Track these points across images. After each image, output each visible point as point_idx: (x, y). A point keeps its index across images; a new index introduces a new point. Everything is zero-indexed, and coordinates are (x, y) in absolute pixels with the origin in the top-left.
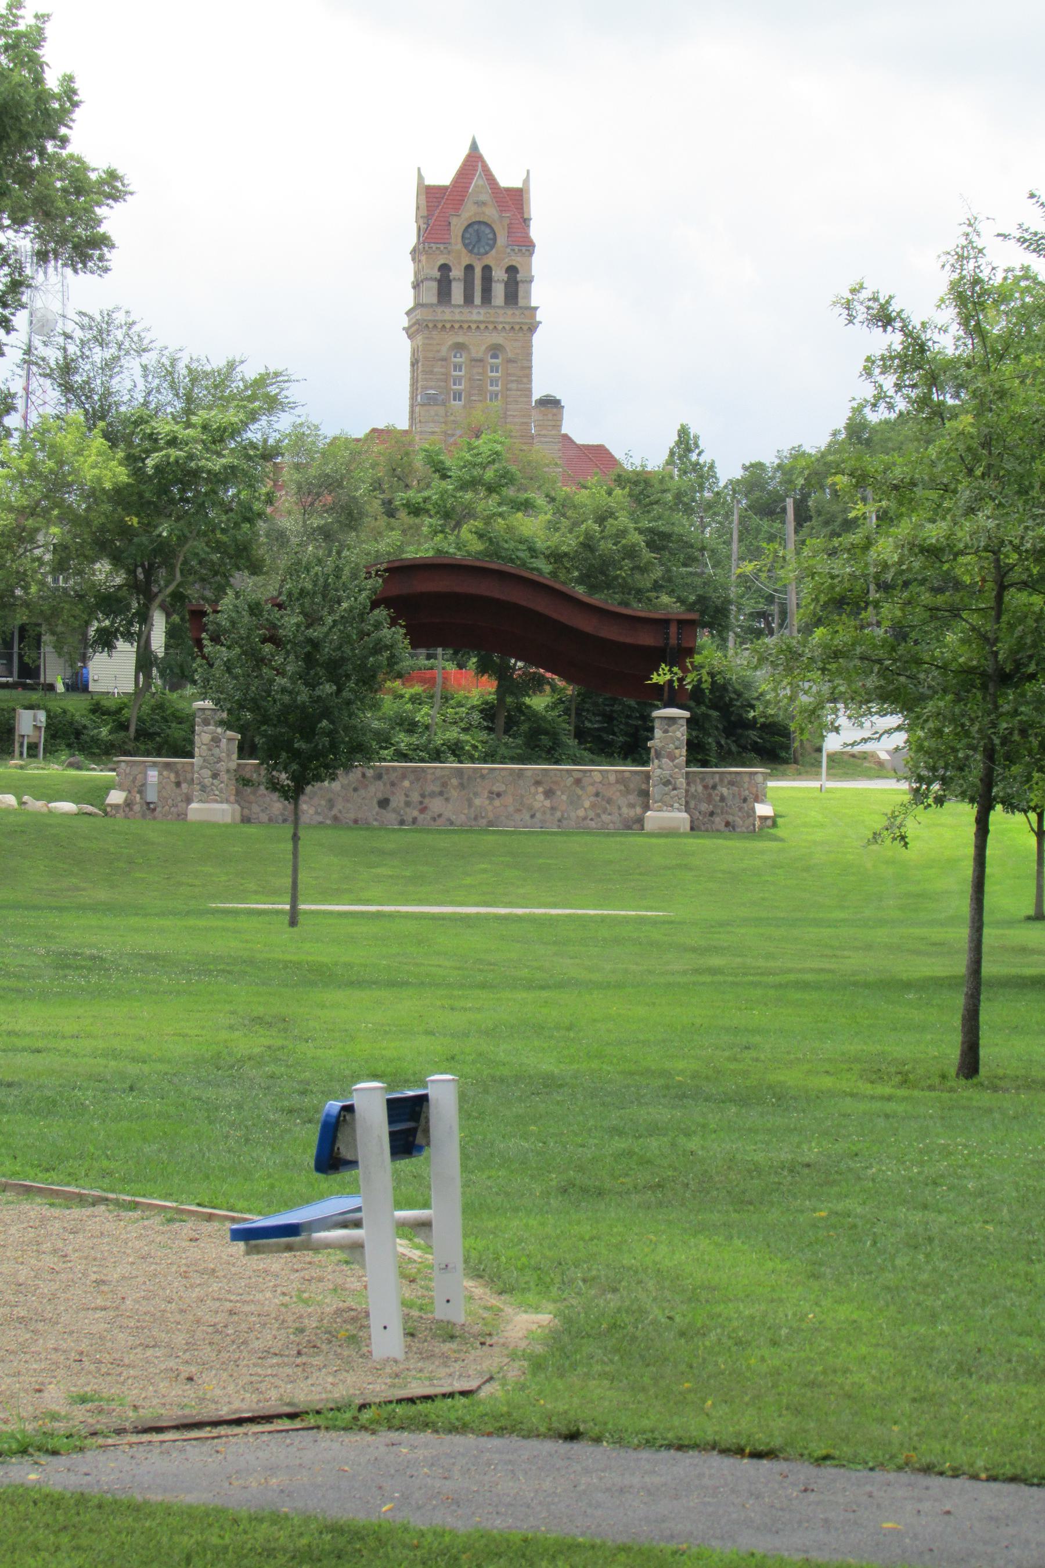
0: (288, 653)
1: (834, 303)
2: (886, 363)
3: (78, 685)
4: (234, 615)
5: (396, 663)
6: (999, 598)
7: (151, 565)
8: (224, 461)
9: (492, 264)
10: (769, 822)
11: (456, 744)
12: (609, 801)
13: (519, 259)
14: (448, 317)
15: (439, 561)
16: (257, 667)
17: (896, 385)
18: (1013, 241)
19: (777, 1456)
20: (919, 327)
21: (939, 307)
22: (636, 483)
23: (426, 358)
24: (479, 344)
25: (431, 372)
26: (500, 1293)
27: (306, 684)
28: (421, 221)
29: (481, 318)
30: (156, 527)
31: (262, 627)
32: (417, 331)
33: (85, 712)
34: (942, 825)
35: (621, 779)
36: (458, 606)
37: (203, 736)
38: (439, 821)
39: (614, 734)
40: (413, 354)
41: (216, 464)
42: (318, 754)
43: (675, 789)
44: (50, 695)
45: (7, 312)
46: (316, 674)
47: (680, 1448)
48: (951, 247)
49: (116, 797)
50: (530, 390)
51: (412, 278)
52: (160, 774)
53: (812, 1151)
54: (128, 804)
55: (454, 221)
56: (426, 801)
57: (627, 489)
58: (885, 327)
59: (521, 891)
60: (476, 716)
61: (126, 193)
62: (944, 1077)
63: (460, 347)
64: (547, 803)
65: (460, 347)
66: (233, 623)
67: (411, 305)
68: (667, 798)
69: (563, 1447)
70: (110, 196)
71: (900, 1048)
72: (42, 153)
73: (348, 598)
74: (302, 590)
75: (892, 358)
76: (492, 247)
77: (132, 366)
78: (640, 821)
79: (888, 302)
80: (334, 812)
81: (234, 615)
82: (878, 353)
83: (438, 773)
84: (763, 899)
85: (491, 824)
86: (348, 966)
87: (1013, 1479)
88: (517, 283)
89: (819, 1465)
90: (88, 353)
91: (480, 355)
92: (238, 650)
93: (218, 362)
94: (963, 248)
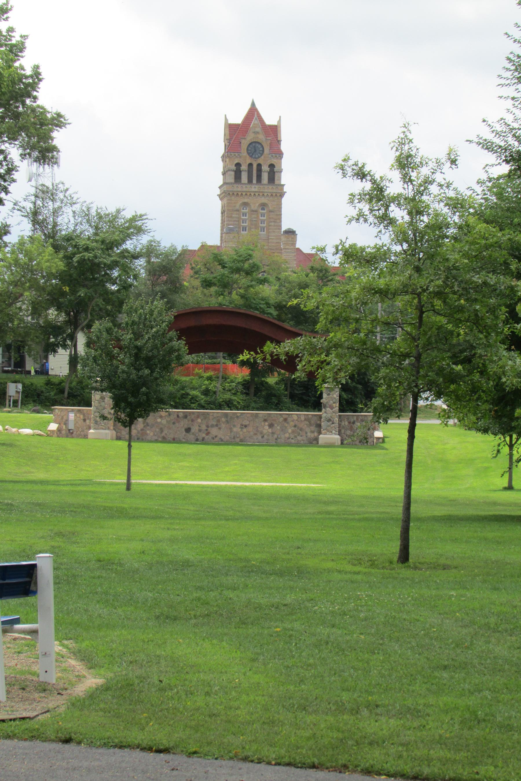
0: (126, 353)
1: (336, 167)
2: (362, 197)
3: (43, 371)
4: (98, 334)
5: (181, 359)
6: (421, 318)
7: (77, 311)
8: (112, 259)
9: (262, 163)
10: (381, 440)
11: (229, 401)
12: (301, 429)
13: (275, 160)
14: (239, 189)
15: (220, 309)
16: (111, 360)
17: (370, 209)
18: (474, 144)
19: (169, 752)
20: (379, 179)
21: (391, 169)
22: (321, 271)
23: (228, 210)
24: (255, 203)
25: (231, 217)
26: (90, 669)
27: (135, 369)
28: (226, 141)
29: (256, 190)
30: (78, 292)
31: (113, 340)
32: (224, 197)
33: (42, 385)
34: (468, 442)
35: (307, 419)
36: (219, 331)
37: (96, 396)
38: (216, 439)
39: (309, 396)
40: (222, 207)
41: (108, 261)
42: (140, 404)
43: (333, 423)
44: (28, 376)
45: (6, 184)
46: (140, 364)
47: (121, 747)
48: (395, 137)
49: (53, 427)
50: (281, 226)
51: (222, 170)
52: (76, 415)
53: (290, 598)
54: (59, 430)
55: (243, 141)
56: (209, 429)
57: (316, 274)
58: (362, 179)
59: (253, 474)
60: (240, 387)
61: (66, 124)
62: (391, 562)
63: (245, 204)
64: (270, 430)
65: (245, 204)
66: (98, 338)
67: (221, 183)
68: (329, 428)
69: (60, 745)
70: (57, 126)
71: (375, 549)
72: (24, 104)
73: (157, 325)
74: (133, 321)
75: (365, 195)
76: (262, 154)
77: (68, 211)
78: (317, 439)
79: (363, 166)
80: (163, 434)
81: (98, 334)
82: (357, 192)
83: (215, 415)
84: (374, 479)
85: (241, 441)
86: (137, 509)
87: (289, 764)
88: (274, 172)
89: (190, 757)
90: (46, 205)
91: (256, 208)
92: (100, 352)
93: (112, 210)
94: (402, 139)
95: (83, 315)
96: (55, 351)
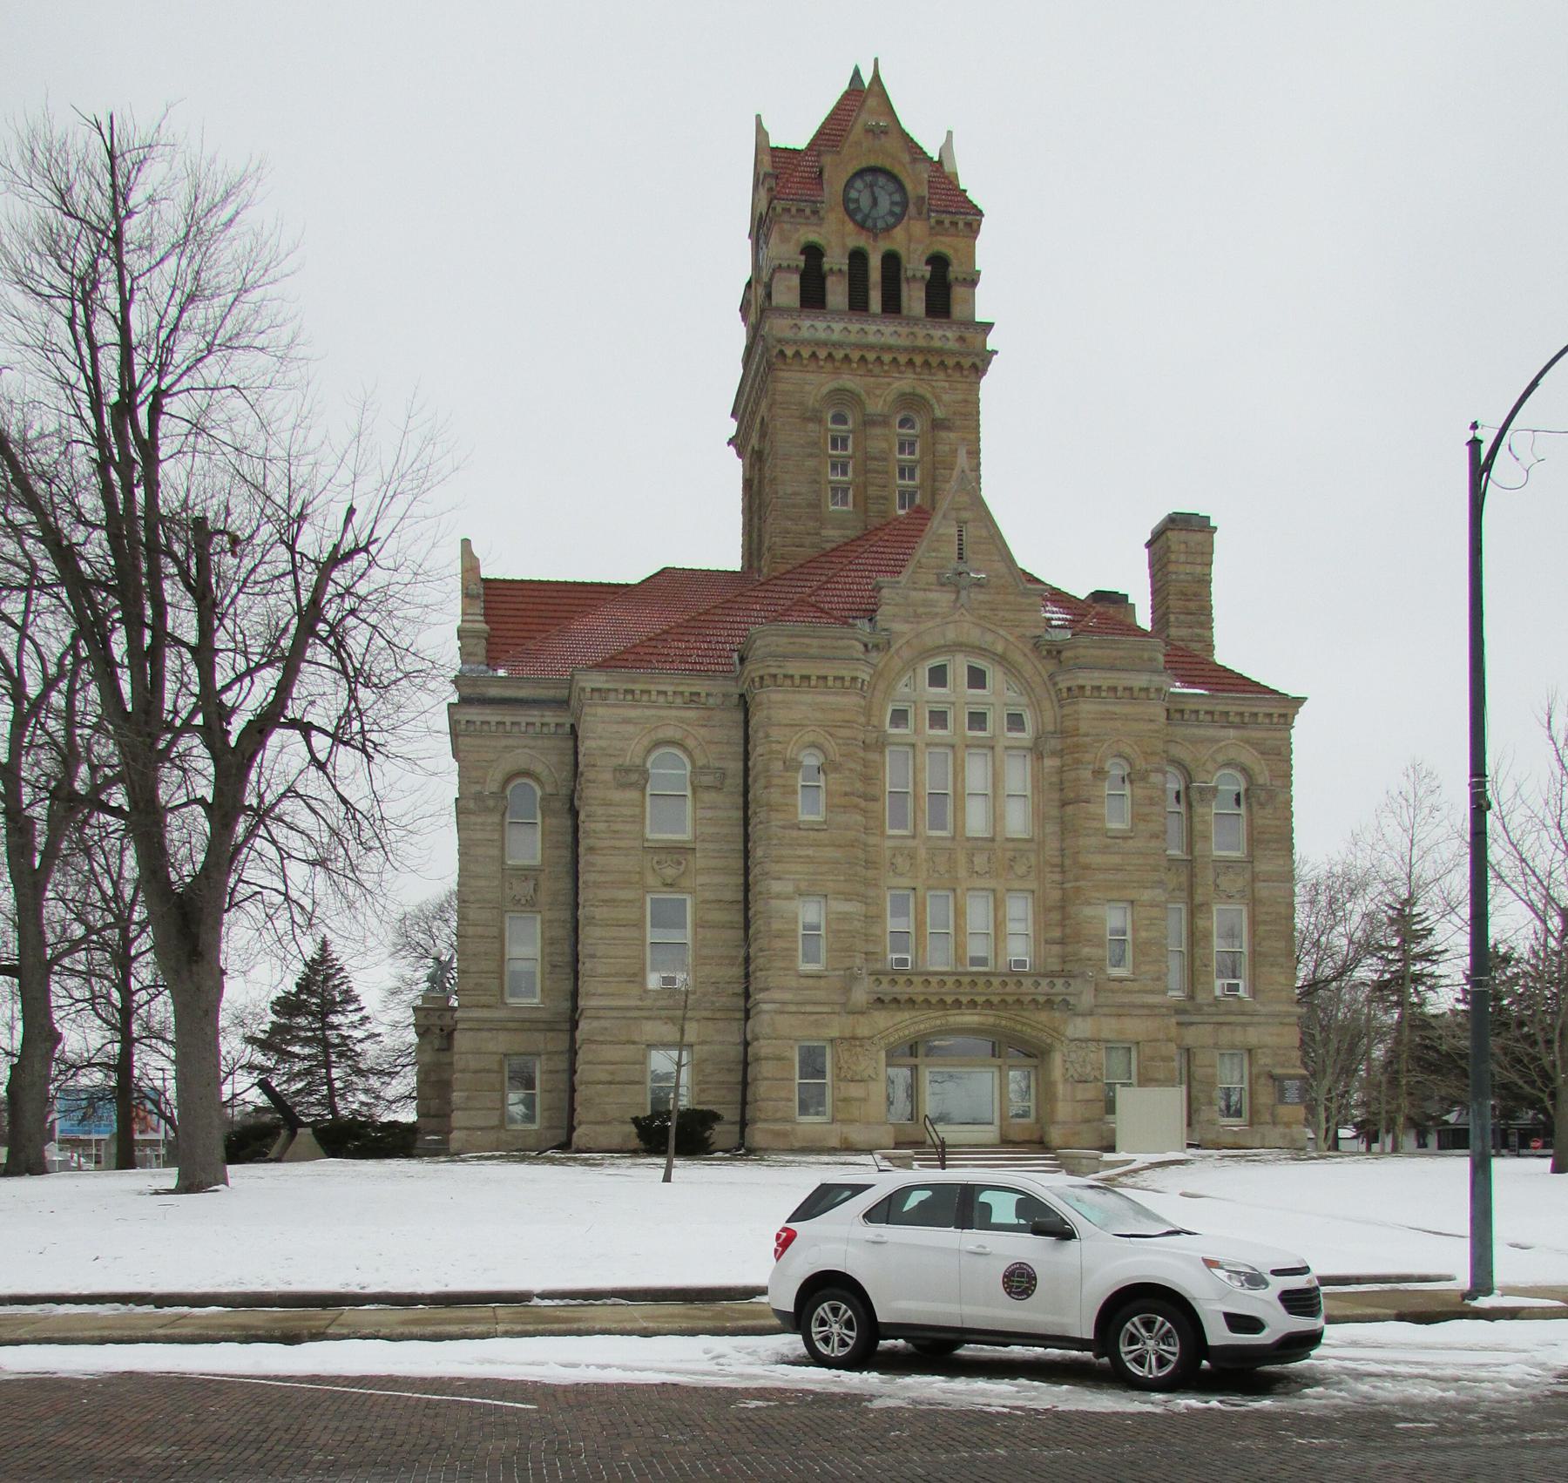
28: (763, 192)
95: (169, 776)
96: (298, 985)
